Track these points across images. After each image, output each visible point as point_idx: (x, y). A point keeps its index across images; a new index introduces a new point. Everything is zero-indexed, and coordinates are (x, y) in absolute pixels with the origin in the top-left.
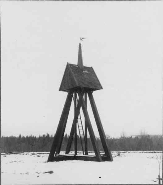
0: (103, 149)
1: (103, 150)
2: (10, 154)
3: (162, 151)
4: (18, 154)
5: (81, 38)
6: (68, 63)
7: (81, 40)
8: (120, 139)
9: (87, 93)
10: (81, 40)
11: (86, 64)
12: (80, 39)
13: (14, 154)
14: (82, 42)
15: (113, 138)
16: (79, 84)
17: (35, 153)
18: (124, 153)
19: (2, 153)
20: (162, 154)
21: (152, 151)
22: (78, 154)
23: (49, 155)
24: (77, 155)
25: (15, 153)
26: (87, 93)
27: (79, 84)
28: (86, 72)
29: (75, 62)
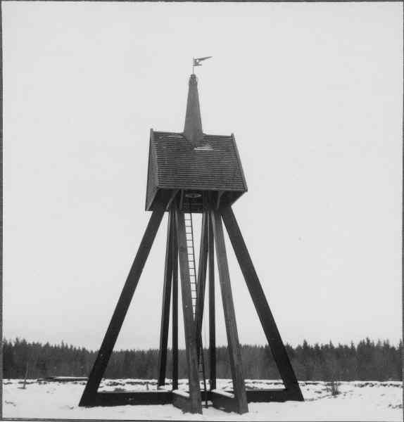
0: (290, 368)
1: (276, 371)
2: (45, 383)
3: (401, 383)
4: (70, 383)
5: (196, 60)
6: (152, 130)
7: (196, 64)
8: (56, 348)
9: (166, 216)
10: (196, 64)
11: (210, 127)
12: (192, 63)
13: (57, 383)
14: (198, 71)
15: (69, 347)
16: (194, 181)
17: (12, 381)
18: (362, 386)
19: (247, 378)
20: (401, 390)
21: (385, 383)
22: (218, 385)
23: (87, 387)
24: (214, 391)
25: (60, 381)
26: (166, 216)
27: (194, 181)
28: (207, 148)
29: (175, 124)
